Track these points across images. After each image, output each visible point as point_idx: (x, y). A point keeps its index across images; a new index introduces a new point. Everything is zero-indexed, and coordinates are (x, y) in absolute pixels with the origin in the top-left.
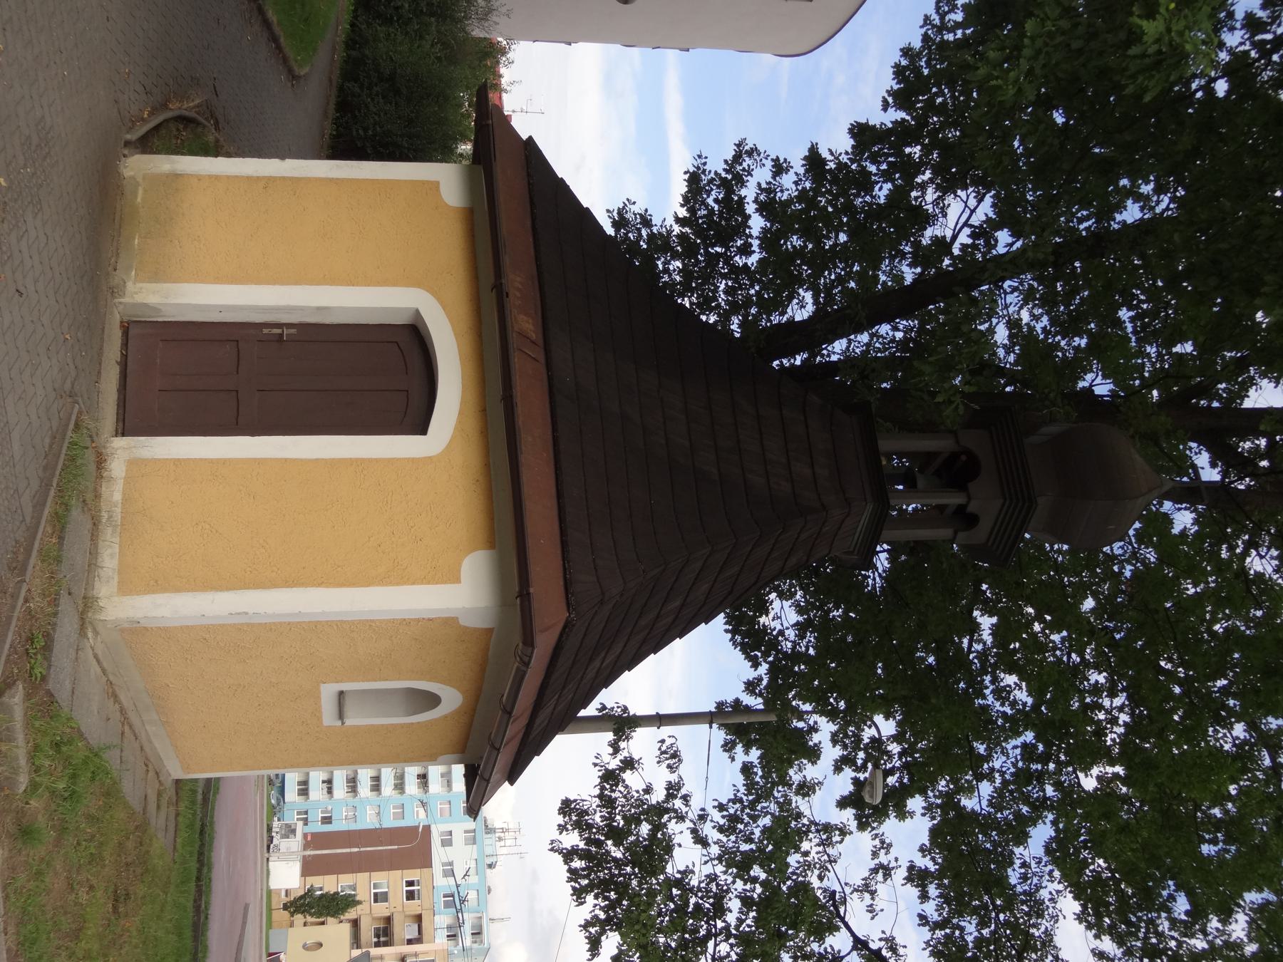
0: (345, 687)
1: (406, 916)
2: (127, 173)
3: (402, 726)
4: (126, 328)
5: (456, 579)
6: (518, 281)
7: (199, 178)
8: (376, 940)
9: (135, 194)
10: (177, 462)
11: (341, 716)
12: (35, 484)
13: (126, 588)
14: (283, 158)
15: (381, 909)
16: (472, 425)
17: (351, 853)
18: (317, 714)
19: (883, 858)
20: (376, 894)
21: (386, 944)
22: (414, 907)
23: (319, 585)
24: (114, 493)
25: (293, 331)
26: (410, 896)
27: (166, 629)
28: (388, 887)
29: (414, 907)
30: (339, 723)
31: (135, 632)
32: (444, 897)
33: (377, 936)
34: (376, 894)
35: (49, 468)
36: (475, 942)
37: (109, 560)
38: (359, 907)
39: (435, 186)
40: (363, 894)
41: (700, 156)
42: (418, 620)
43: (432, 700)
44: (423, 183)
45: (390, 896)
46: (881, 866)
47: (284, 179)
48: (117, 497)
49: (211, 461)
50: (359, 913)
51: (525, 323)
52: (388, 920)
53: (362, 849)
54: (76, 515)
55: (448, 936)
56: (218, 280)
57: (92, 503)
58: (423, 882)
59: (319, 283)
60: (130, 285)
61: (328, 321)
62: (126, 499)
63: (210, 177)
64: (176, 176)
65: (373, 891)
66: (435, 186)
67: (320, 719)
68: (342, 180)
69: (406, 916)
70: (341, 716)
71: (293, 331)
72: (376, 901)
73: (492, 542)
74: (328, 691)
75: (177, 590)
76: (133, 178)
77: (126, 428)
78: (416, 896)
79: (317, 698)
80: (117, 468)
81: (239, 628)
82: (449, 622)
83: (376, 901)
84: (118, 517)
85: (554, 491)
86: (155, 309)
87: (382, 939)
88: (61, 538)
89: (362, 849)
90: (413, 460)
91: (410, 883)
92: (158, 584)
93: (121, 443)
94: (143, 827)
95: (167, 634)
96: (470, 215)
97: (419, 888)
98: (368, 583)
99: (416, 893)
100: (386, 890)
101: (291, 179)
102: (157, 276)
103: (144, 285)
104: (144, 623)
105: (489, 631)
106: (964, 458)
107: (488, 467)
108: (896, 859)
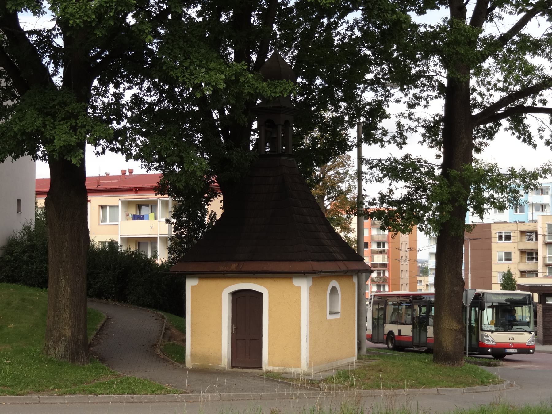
0: (328, 312)
1: (521, 241)
2: (191, 367)
3: (342, 295)
4: (233, 367)
5: (299, 288)
6: (222, 268)
7: (192, 349)
8: (535, 260)
9: (196, 365)
10: (269, 354)
11: (337, 313)
12: (276, 383)
13: (299, 366)
14: (185, 327)
15: (516, 256)
16: (261, 281)
17: (472, 278)
18: (336, 320)
19: (407, 115)
20: (506, 260)
21: (537, 254)
22: (515, 235)
23: (300, 321)
24: (276, 369)
25: (234, 325)
26: (508, 238)
27: (310, 357)
28: (502, 252)
29: (515, 235)
30: (340, 314)
31: (310, 364)
32: (517, 212)
33: (532, 259)
34: (506, 260)
35: (272, 381)
36: (548, 192)
37: (293, 370)
38: (511, 271)
39: (192, 287)
40: (504, 267)
41: (141, 167)
42: (310, 297)
43: (334, 289)
44: (191, 290)
45: (508, 250)
46: (409, 115)
47: (191, 327)
48: (277, 368)
49: (269, 346)
50: (516, 270)
51: (234, 266)
52: (522, 252)
53: (470, 271)
54: (283, 376)
55: (542, 210)
56: (221, 344)
57: (279, 374)
58: (500, 230)
59: (221, 319)
60: (222, 366)
61: (231, 316)
62: (278, 366)
63: (191, 346)
64: (192, 355)
65: (504, 261)
66: (192, 287)
67: (338, 319)
68: (300, 338)
69: (521, 241)
70: (337, 313)
71: (234, 325)
72: (510, 260)
73: (291, 278)
74: (329, 317)
75: (300, 354)
76: (192, 366)
77: (261, 367)
78: (508, 234)
79: (331, 320)
80: (270, 368)
81: (310, 340)
82: (310, 289)
83: (510, 260)
84: (281, 368)
85: (278, 262)
86: (229, 359)
87: (534, 256)
88: (288, 378)
89: (470, 271)
90: (269, 296)
91: (500, 238)
92: (299, 359)
93: (264, 368)
94: (364, 366)
95: (311, 357)
96: (200, 278)
97: (503, 232)
98: (300, 309)
99: (507, 234)
100: (503, 254)
101: (191, 325)
102: (220, 360)
103: (222, 362)
104: (308, 362)
105: (313, 278)
106: (267, 123)
107: (271, 278)
108: (407, 111)
